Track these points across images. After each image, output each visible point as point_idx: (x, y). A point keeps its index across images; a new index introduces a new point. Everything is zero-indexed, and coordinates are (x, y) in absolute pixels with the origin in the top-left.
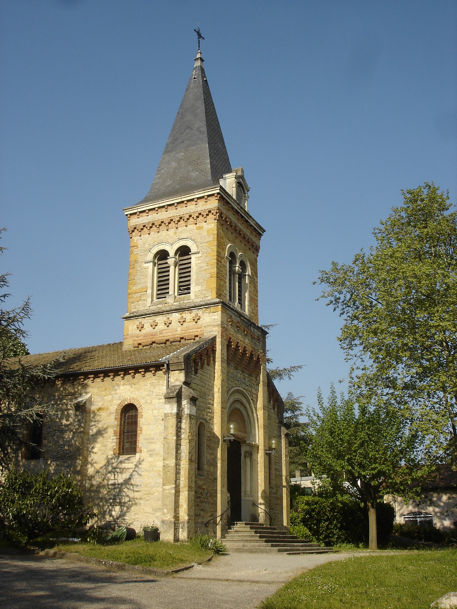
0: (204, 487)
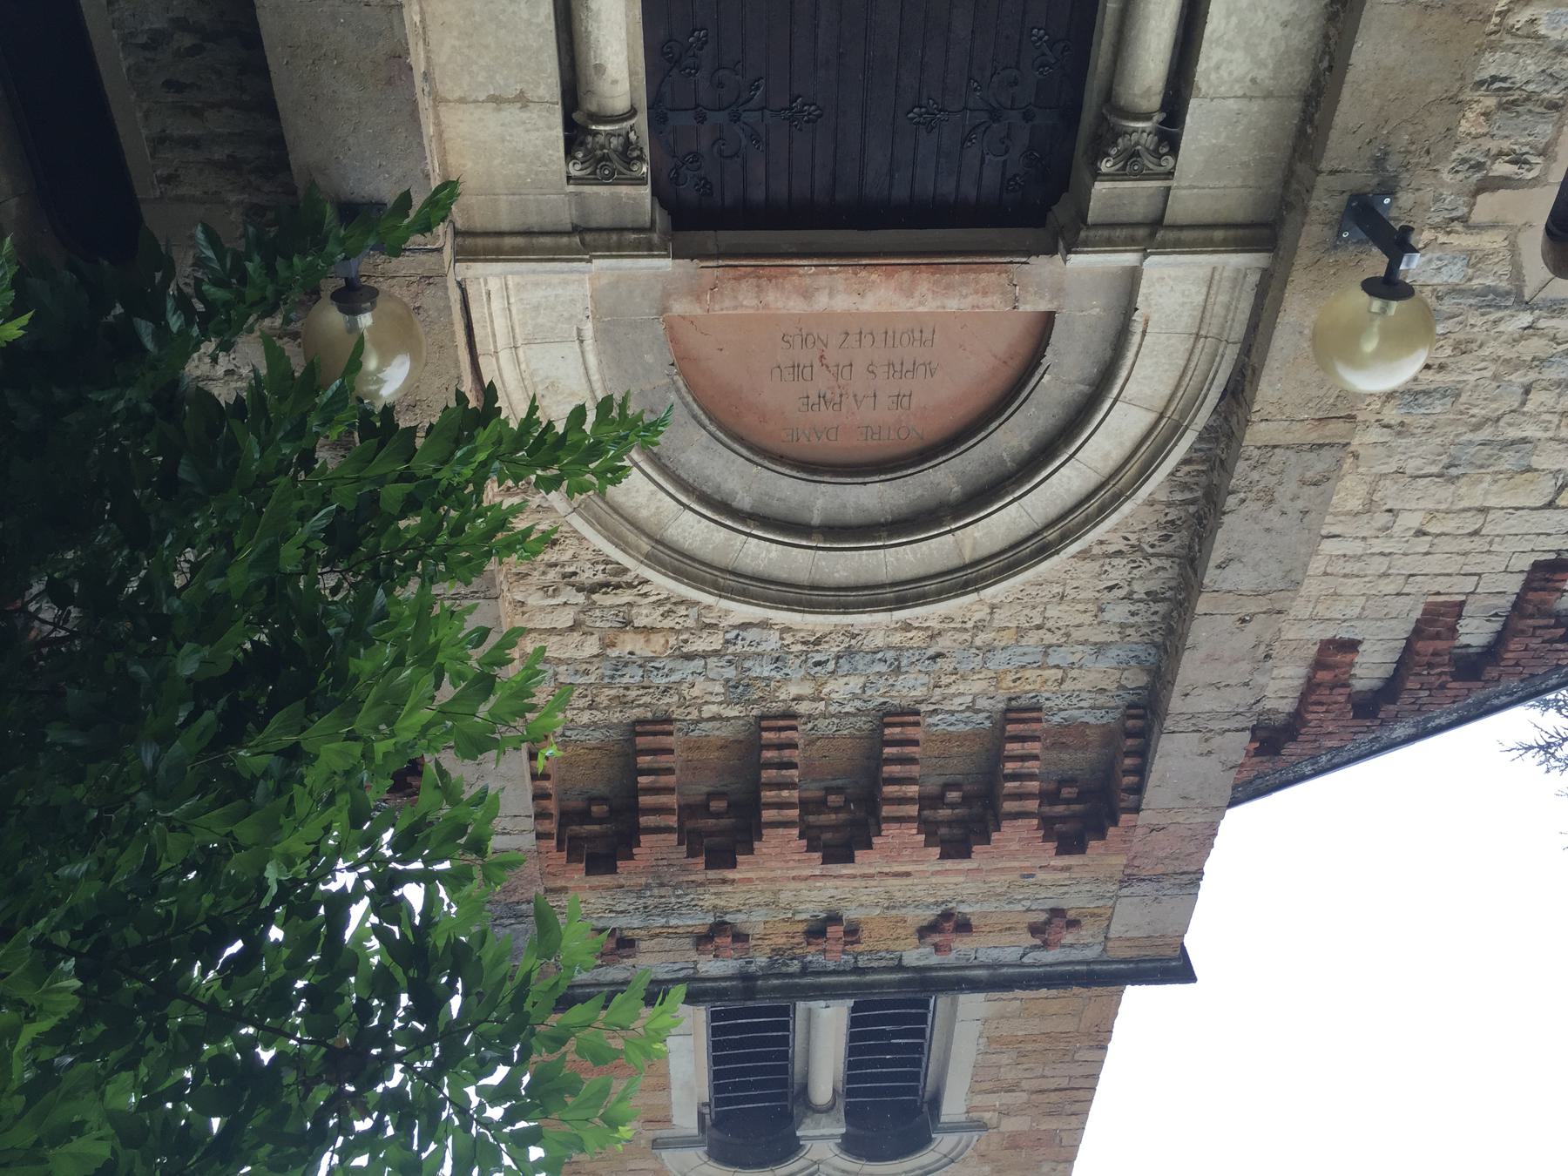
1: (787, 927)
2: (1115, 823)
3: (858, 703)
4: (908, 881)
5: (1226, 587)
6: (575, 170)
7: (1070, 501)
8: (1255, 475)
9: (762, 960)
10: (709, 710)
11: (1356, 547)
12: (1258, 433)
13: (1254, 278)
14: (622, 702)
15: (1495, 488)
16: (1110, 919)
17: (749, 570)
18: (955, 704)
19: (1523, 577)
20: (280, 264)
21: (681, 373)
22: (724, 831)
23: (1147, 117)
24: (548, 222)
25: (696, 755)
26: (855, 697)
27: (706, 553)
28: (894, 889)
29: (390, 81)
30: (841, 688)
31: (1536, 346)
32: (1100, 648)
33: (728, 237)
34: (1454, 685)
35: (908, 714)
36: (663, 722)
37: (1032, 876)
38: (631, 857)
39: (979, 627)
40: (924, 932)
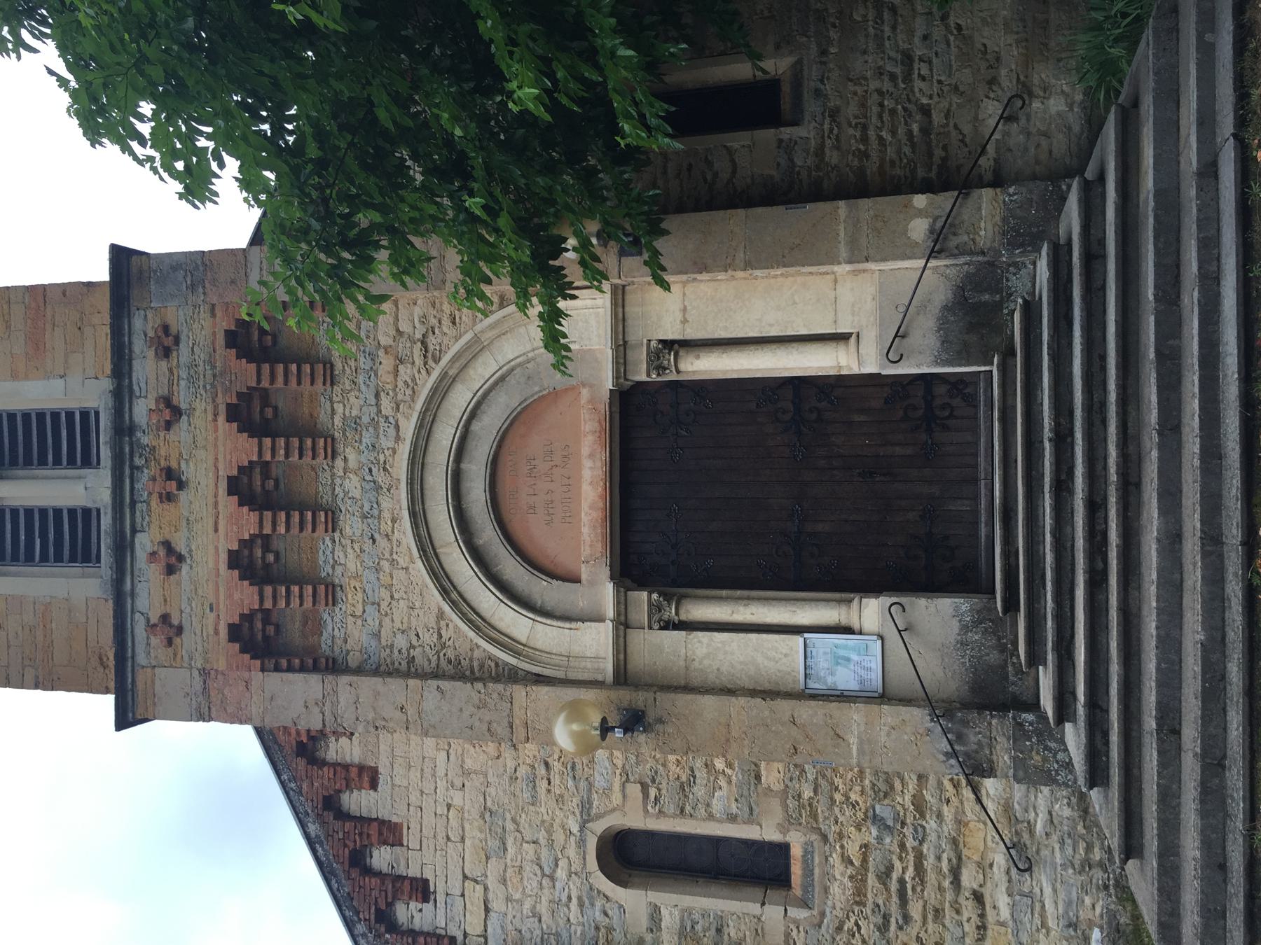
0: (853, 850)
1: (174, 455)
2: (252, 658)
3: (341, 495)
4: (211, 530)
5: (425, 693)
6: (653, 344)
7: (474, 604)
8: (495, 696)
9: (145, 440)
10: (339, 408)
11: (441, 771)
12: (519, 691)
13: (600, 678)
14: (345, 359)
15: (477, 841)
16: (171, 666)
17: (435, 428)
18: (339, 553)
19: (419, 876)
20: (643, 217)
21: (549, 393)
22: (250, 414)
23: (677, 614)
24: (629, 330)
25: (306, 399)
26: (346, 493)
27: (446, 405)
28: (207, 525)
29: (695, 263)
30: (353, 485)
31: (559, 837)
32: (377, 635)
33: (617, 417)
34: (347, 851)
35: (333, 524)
36: (331, 379)
37: (211, 609)
38: (238, 357)
39: (393, 562)
40: (167, 545)
